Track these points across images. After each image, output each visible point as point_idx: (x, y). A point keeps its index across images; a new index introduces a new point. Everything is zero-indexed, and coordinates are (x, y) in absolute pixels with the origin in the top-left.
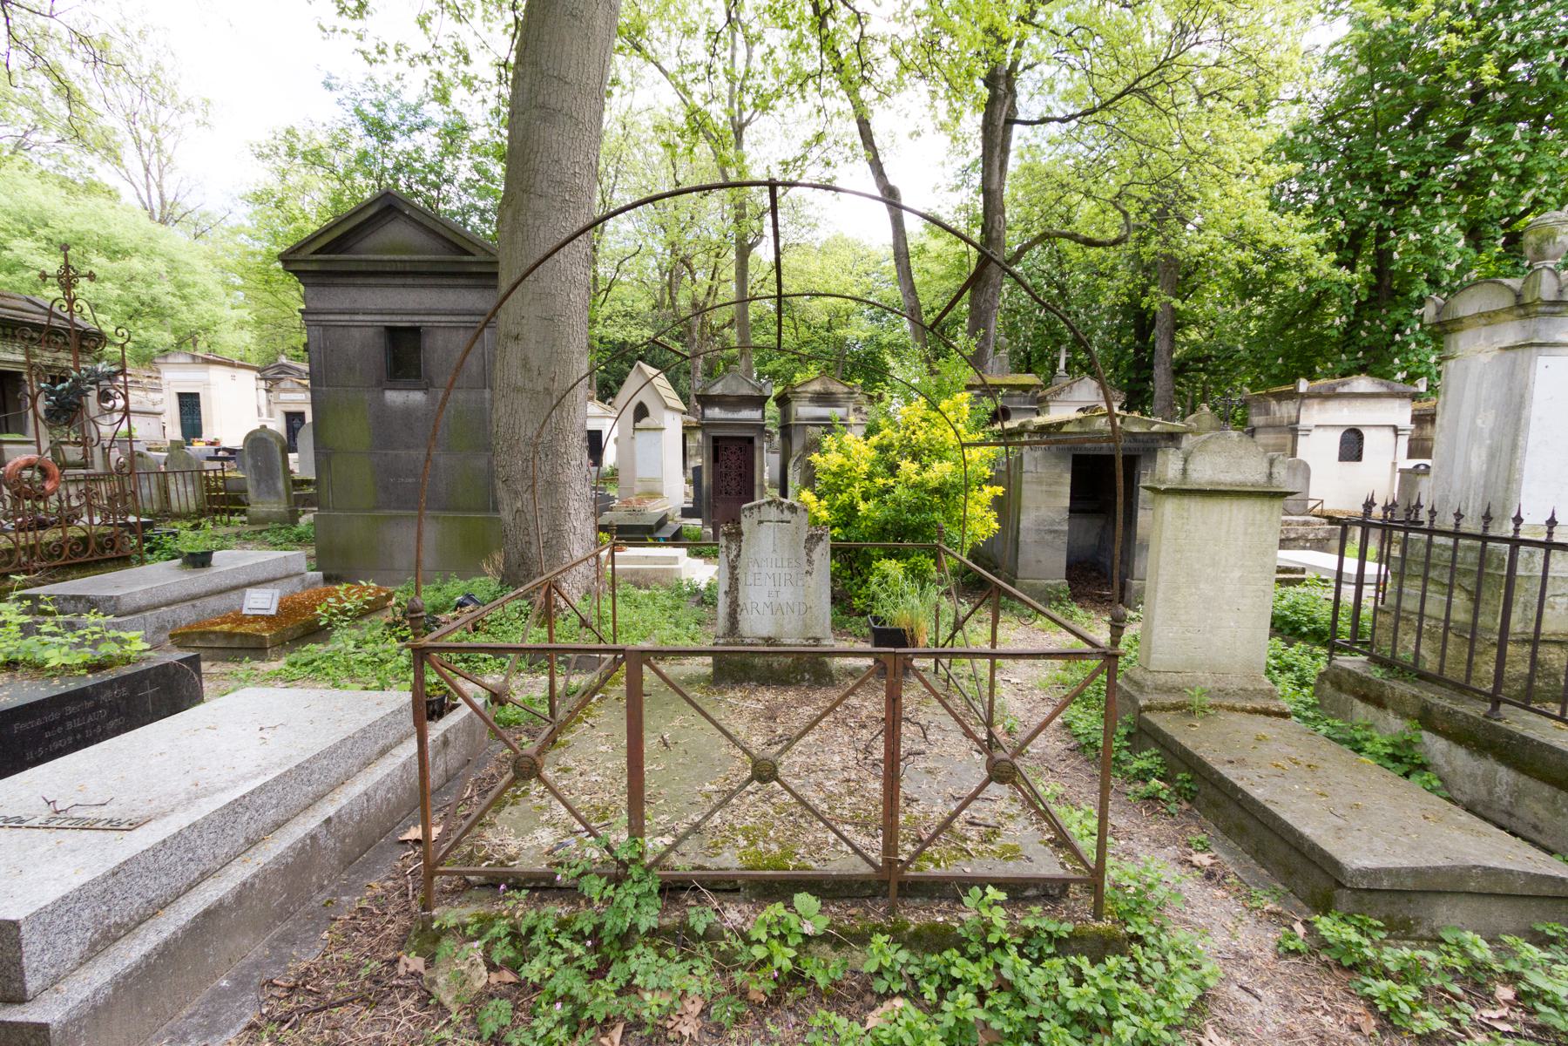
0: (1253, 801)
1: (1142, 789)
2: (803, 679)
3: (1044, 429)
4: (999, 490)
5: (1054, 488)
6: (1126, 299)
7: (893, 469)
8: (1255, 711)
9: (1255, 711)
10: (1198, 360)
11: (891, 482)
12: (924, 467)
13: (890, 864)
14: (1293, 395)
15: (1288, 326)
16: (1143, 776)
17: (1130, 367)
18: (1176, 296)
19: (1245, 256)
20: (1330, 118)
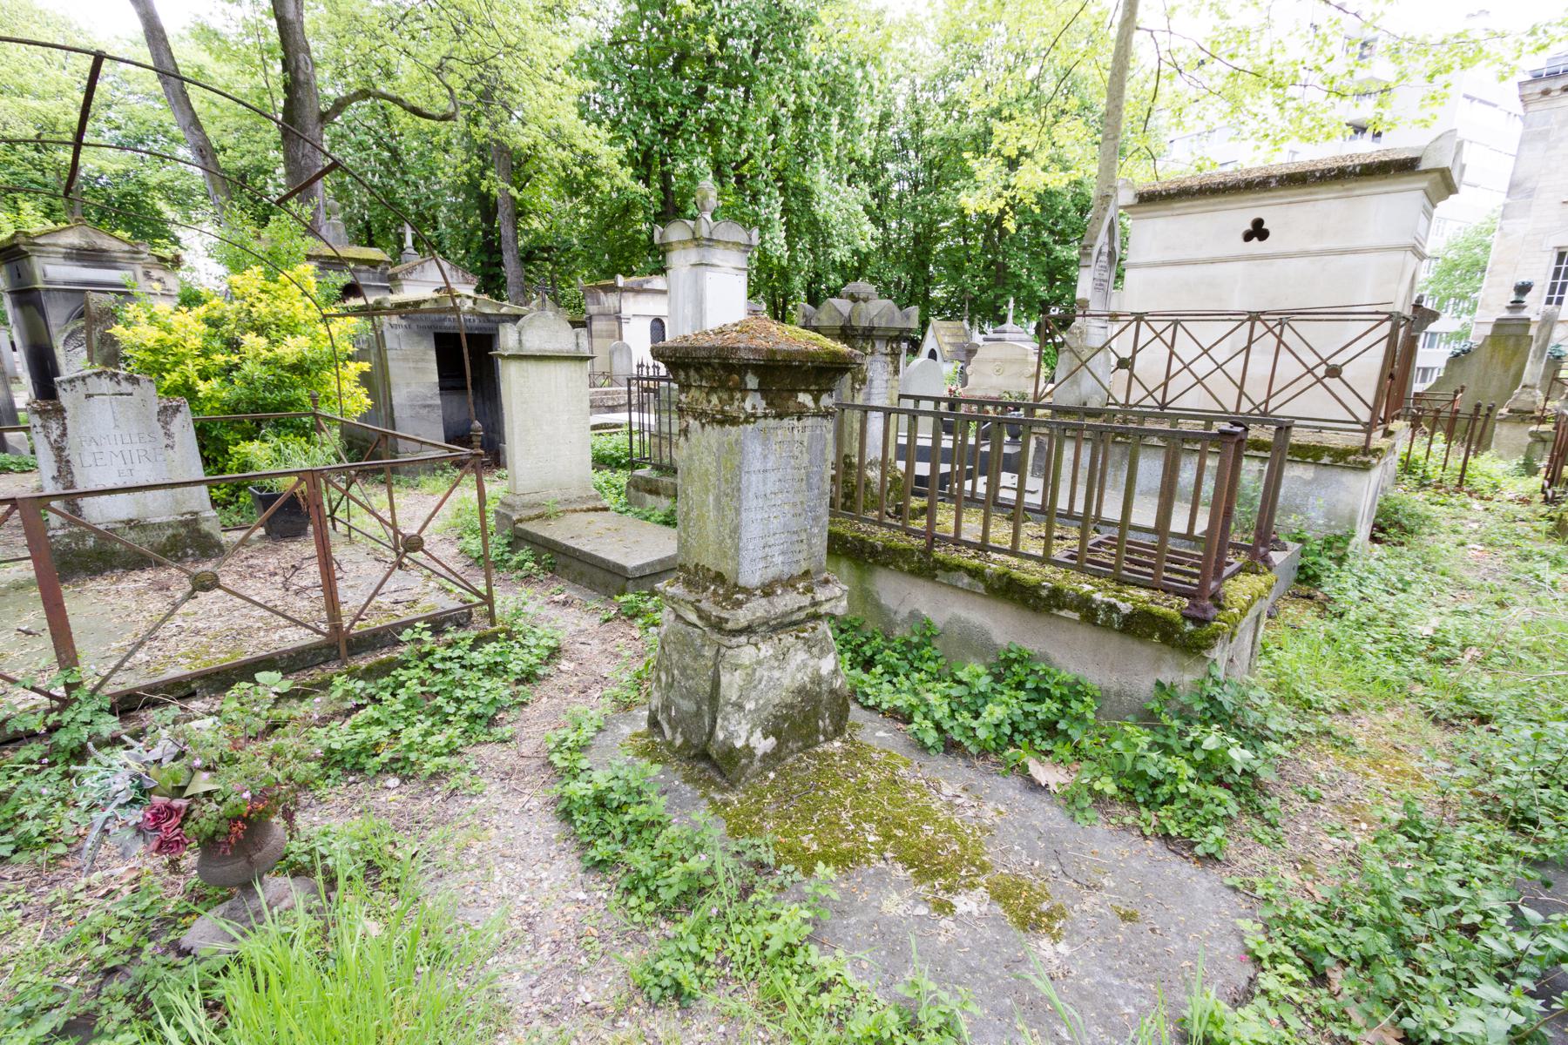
0: (585, 554)
1: (521, 573)
2: (186, 555)
3: (400, 308)
4: (366, 366)
5: (420, 365)
6: (465, 179)
7: (233, 345)
8: (589, 510)
9: (589, 510)
10: (543, 250)
11: (235, 359)
12: (273, 342)
13: (336, 628)
14: (613, 289)
15: (609, 226)
16: (520, 565)
17: (481, 250)
18: (513, 184)
19: (566, 155)
20: (616, 43)
